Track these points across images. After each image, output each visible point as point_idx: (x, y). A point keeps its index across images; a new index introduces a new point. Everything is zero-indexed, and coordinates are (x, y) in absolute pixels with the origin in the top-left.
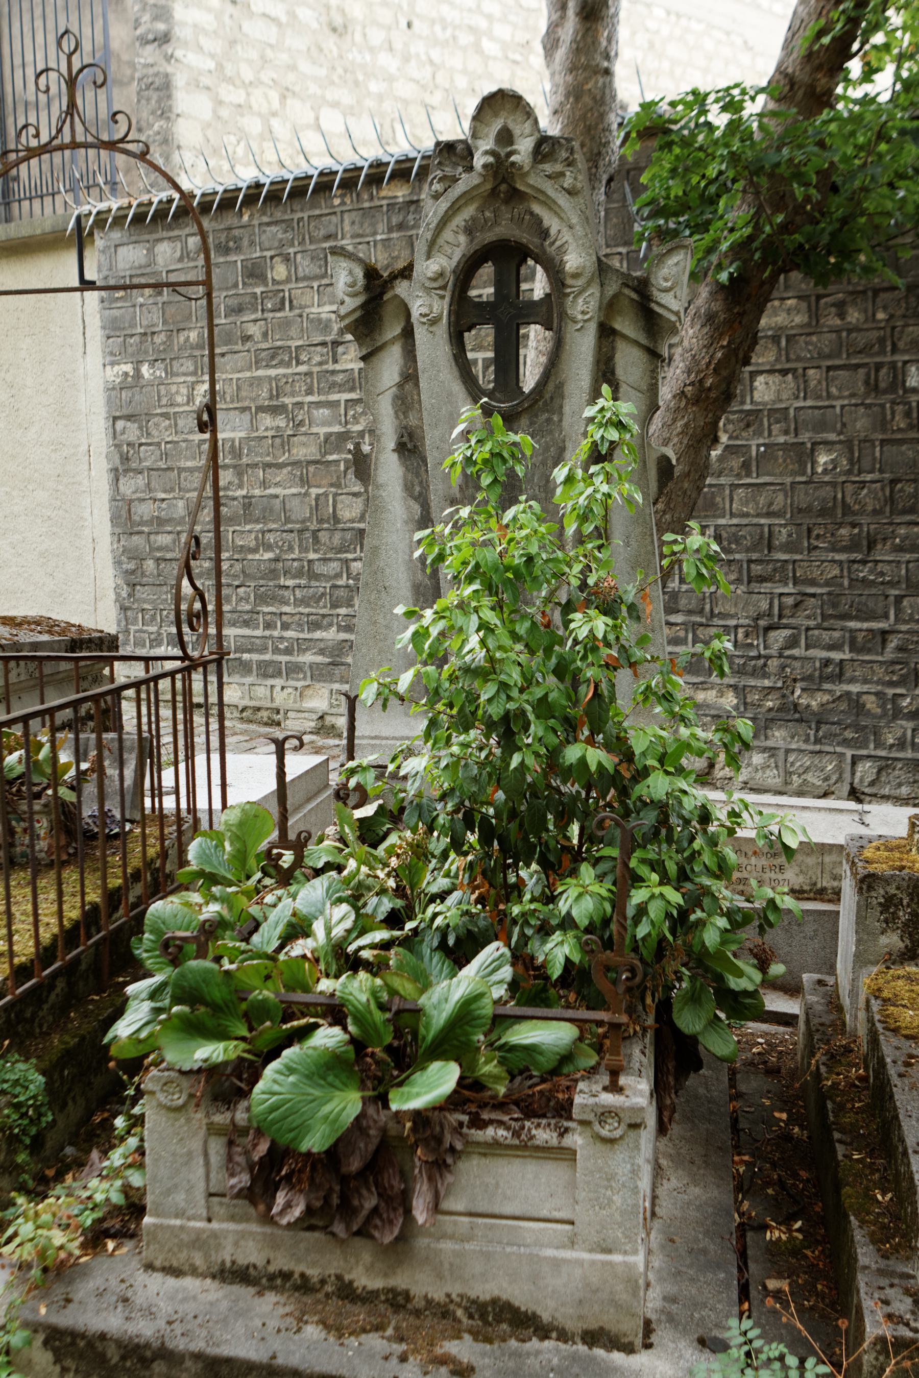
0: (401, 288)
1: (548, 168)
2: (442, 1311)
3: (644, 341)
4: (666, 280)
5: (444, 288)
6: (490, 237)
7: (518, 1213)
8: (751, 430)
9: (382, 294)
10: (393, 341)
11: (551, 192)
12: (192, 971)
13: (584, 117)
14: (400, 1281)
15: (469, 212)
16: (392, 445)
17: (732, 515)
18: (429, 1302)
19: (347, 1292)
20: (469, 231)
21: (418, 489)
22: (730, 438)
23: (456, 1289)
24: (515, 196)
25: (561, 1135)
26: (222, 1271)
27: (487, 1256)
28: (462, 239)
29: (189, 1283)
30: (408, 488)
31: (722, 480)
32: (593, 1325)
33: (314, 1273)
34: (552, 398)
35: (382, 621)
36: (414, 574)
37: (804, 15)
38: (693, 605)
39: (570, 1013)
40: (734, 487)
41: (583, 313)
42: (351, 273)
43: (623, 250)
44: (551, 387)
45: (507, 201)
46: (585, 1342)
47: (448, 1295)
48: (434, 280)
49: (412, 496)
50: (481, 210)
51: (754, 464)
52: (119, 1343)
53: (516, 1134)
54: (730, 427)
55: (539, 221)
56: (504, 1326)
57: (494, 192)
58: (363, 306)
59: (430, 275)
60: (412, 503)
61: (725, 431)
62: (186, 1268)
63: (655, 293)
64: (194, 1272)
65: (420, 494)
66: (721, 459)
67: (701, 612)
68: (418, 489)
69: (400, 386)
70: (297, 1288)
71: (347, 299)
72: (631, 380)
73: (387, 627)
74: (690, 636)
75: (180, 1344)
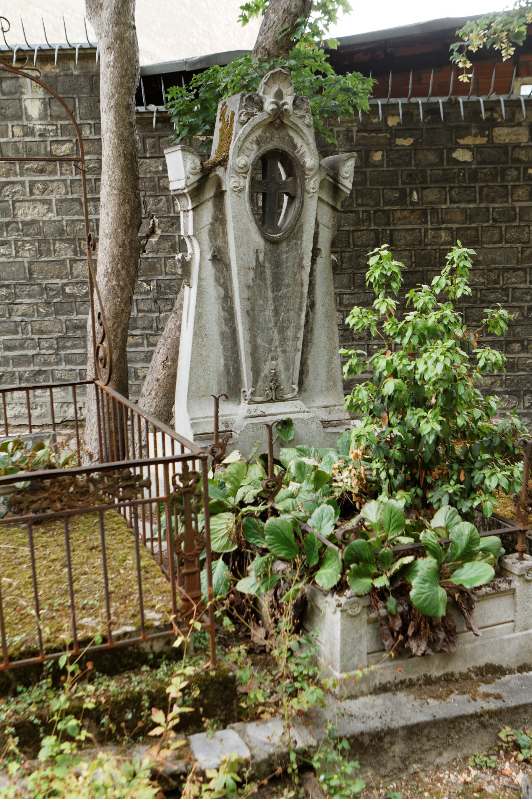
0: (220, 171)
1: (299, 113)
2: (465, 677)
3: (331, 203)
4: (347, 173)
5: (246, 173)
6: (270, 146)
7: (494, 623)
8: (174, 227)
9: (209, 174)
10: (208, 200)
11: (300, 126)
12: (356, 546)
13: (126, 53)
14: (450, 669)
15: (258, 133)
16: (209, 257)
17: (166, 274)
18: (461, 674)
19: (428, 681)
20: (259, 142)
21: (222, 280)
22: (162, 231)
23: (471, 665)
24: (282, 126)
25: (510, 584)
26: (375, 690)
27: (484, 646)
28: (255, 147)
29: (362, 700)
30: (217, 280)
31: (160, 255)
32: (521, 663)
33: (414, 677)
35: (204, 353)
36: (221, 327)
37: (275, 19)
38: (146, 324)
39: (493, 532)
40: (166, 258)
41: (313, 189)
42: (193, 162)
43: (92, 122)
44: (297, 227)
45: (277, 129)
46: (519, 671)
47: (469, 669)
48: (241, 168)
50: (264, 132)
51: (177, 246)
52: (369, 734)
53: (493, 588)
54: (162, 226)
55: (292, 139)
56: (489, 675)
57: (271, 124)
58: (199, 181)
59: (240, 165)
61: (159, 228)
62: (359, 693)
63: (341, 179)
64: (363, 694)
65: (224, 283)
66: (158, 243)
67: (151, 328)
68: (222, 280)
69: (212, 224)
70: (408, 687)
71: (191, 176)
73: (207, 356)
74: (145, 342)
75: (395, 725)
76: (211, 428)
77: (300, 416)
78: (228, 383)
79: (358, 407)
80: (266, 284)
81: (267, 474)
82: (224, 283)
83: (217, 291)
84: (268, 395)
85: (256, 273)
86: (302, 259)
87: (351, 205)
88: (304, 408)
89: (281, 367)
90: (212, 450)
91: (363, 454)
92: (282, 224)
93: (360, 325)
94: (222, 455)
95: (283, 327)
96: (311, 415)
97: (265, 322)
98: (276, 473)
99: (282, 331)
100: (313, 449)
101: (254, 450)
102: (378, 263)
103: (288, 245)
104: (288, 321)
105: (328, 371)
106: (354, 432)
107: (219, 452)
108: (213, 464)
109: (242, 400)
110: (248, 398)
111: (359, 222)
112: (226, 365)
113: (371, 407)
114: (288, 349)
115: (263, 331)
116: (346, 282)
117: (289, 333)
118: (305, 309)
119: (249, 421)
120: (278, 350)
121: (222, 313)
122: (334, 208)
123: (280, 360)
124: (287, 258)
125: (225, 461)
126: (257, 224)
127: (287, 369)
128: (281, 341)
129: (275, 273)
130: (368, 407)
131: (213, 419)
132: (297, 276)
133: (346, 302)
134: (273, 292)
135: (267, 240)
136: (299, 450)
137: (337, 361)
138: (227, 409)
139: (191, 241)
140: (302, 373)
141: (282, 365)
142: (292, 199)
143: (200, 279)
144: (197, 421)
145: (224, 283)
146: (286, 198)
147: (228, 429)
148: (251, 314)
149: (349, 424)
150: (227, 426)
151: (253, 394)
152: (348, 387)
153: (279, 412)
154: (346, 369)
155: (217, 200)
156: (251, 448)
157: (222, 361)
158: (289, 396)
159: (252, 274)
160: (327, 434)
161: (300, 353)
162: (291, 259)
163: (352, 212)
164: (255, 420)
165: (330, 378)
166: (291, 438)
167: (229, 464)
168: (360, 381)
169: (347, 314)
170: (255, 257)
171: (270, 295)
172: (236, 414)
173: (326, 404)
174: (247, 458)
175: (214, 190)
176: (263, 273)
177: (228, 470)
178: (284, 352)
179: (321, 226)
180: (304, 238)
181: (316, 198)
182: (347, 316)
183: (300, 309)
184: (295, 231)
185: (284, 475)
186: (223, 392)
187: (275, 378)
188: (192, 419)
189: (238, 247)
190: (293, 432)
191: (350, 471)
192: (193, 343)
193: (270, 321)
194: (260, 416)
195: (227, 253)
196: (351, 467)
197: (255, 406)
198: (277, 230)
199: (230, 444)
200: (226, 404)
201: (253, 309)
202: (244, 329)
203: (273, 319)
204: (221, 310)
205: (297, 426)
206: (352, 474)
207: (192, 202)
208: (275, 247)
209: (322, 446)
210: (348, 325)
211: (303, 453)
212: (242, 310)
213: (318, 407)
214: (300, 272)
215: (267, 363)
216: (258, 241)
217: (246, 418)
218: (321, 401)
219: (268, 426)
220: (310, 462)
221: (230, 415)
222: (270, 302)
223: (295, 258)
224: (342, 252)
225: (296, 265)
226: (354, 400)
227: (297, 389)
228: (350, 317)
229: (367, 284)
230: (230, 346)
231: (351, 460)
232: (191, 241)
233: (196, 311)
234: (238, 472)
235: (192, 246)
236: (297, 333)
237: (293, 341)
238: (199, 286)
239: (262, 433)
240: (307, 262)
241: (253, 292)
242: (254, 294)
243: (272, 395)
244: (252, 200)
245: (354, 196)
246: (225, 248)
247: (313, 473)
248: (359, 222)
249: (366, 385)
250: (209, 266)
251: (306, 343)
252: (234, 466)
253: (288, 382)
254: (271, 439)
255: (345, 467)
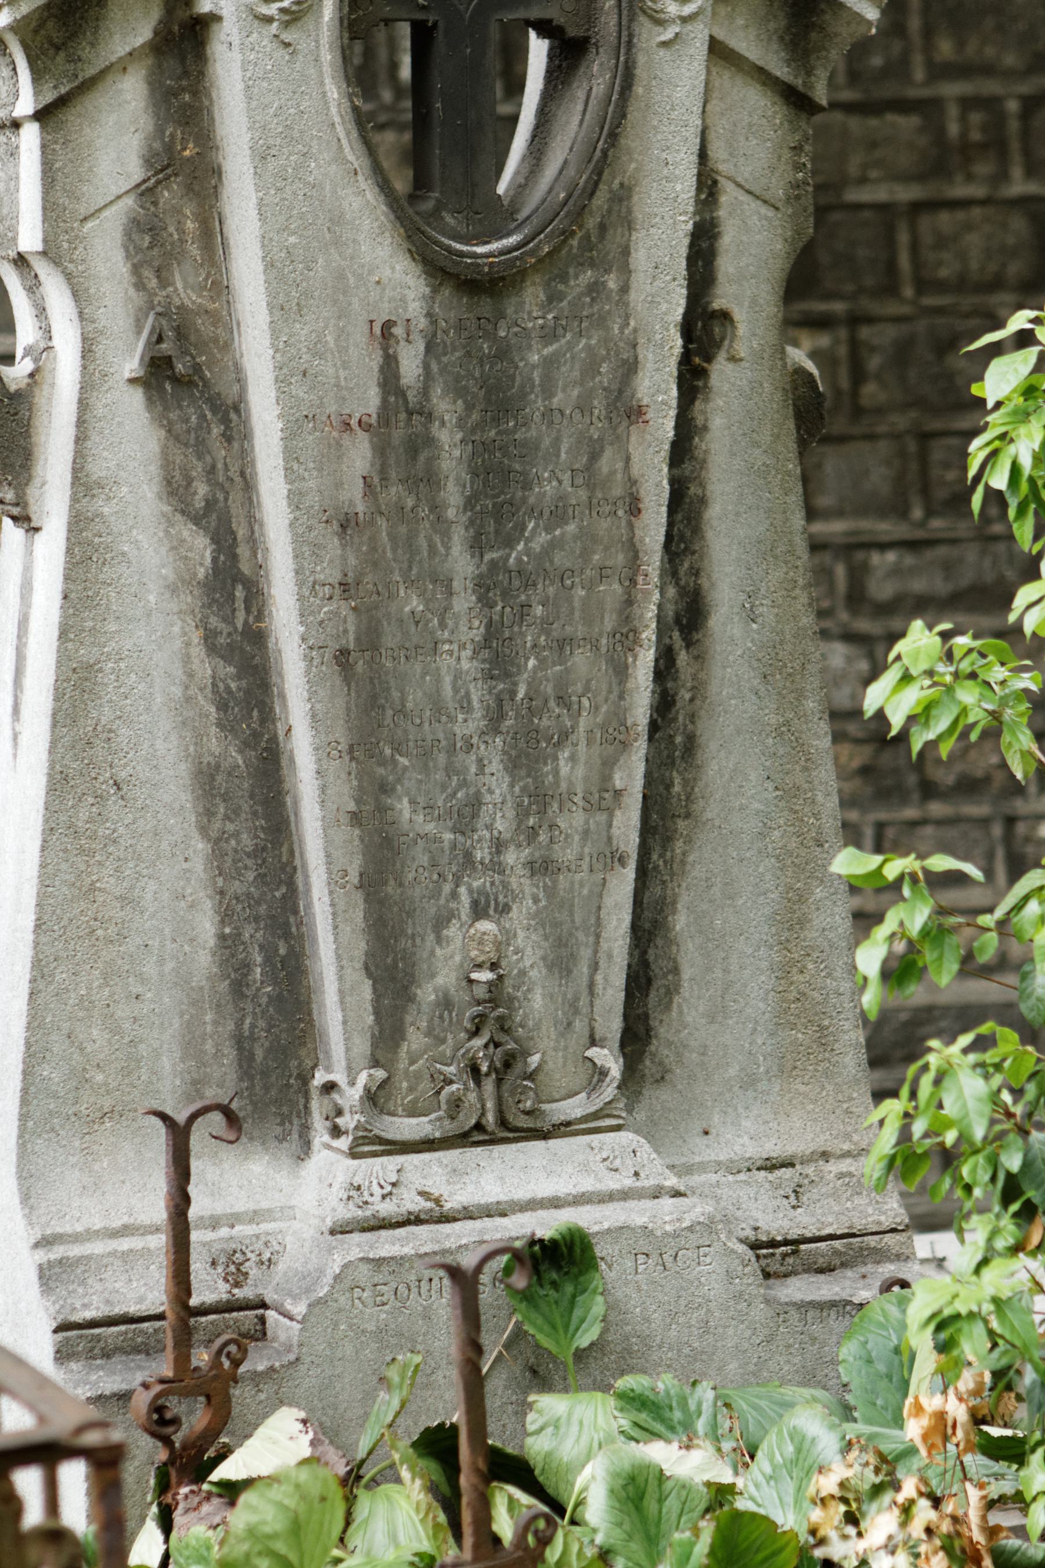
3: (781, 70)
10: (121, 66)
16: (132, 365)
21: (202, 489)
30: (175, 489)
34: (603, 228)
35: (108, 883)
36: (199, 738)
44: (600, 200)
49: (185, 511)
60: (187, 531)
65: (210, 504)
68: (202, 489)
69: (146, 192)
72: (745, 172)
73: (124, 900)
76: (147, 1291)
77: (636, 1214)
78: (242, 1043)
79: (948, 1158)
80: (436, 508)
81: (458, 1536)
82: (212, 500)
83: (177, 546)
84: (456, 1104)
85: (381, 450)
86: (630, 368)
87: (898, 69)
88: (657, 1172)
89: (528, 953)
90: (158, 1409)
91: (978, 1419)
92: (521, 188)
93: (941, 724)
94: (211, 1433)
95: (533, 735)
96: (696, 1210)
97: (439, 709)
98: (504, 1526)
99: (528, 756)
100: (705, 1394)
101: (388, 1403)
102: (1029, 391)
103: (553, 298)
104: (562, 700)
105: (785, 971)
106: (925, 1300)
107: (194, 1418)
108: (164, 1486)
109: (320, 1136)
110: (347, 1121)
111: (941, 160)
112: (228, 944)
113: (1013, 1162)
114: (566, 854)
115: (425, 754)
116: (879, 478)
117: (571, 768)
118: (649, 634)
119: (357, 1245)
120: (511, 857)
121: (204, 668)
122: (797, 100)
123: (519, 915)
124: (550, 363)
125: (227, 1471)
126: (384, 186)
127: (560, 963)
128: (522, 814)
129: (486, 447)
130: (994, 1163)
131: (160, 1242)
132: (609, 461)
133: (881, 589)
134: (477, 546)
135: (441, 271)
136: (632, 1401)
137: (833, 916)
138: (233, 1183)
139: (33, 285)
140: (641, 981)
141: (534, 940)
142: (569, 53)
143: (82, 483)
144: (75, 1251)
145: (212, 500)
146: (538, 51)
147: (245, 1293)
148: (358, 664)
149: (904, 1257)
150: (237, 1277)
151: (375, 1099)
152: (894, 1049)
153: (522, 1194)
154: (870, 958)
155: (171, 63)
156: (369, 1397)
157: (206, 926)
158: (574, 1108)
159: (359, 456)
160: (782, 1310)
161: (630, 873)
162: (568, 372)
163: (902, 106)
164: (389, 1245)
165: (800, 1010)
166: (584, 1340)
167: (248, 1483)
168: (961, 1018)
169: (874, 652)
170: (376, 361)
171: (462, 564)
172: (287, 1212)
173: (772, 1148)
174: (344, 1449)
175: (156, 14)
176: (420, 445)
177: (240, 1518)
178: (542, 867)
179: (729, 195)
180: (640, 258)
181: (699, 48)
182: (873, 676)
183: (626, 637)
184: (589, 222)
185: (544, 1541)
186: (213, 1094)
187: (493, 1012)
188: (44, 1242)
189: (284, 310)
190: (598, 1307)
191: (907, 1510)
192: (49, 831)
193: (466, 707)
194: (414, 1220)
195: (227, 346)
196: (909, 1488)
197: (387, 1166)
198: (495, 218)
199: (256, 1378)
200: (228, 1155)
201: (370, 639)
202: (323, 750)
203: (477, 693)
204: (198, 651)
205: (617, 1272)
206: (917, 1529)
207: (38, 76)
208: (486, 306)
209: (755, 1376)
210: (880, 715)
211: (652, 1415)
212: (312, 649)
213: (732, 1168)
214: (621, 442)
215: (452, 931)
216: (392, 278)
217: (340, 1230)
218: (745, 1136)
219: (455, 1273)
220: (688, 1464)
221: (255, 1216)
222: (464, 602)
223: (591, 368)
224: (855, 320)
225: (599, 405)
226: (918, 1128)
227: (615, 1068)
228: (890, 678)
229: (977, 501)
230: (247, 841)
231: (911, 1451)
232: (33, 285)
233: (63, 658)
234: (296, 1528)
235: (41, 312)
236: (608, 765)
237: (590, 807)
238: (79, 524)
239: (427, 1315)
240: (657, 385)
241: (371, 550)
242: (373, 561)
243: (482, 1102)
244: (362, 73)
245: (915, 24)
246: (215, 318)
247: (708, 1529)
248: (941, 160)
249: (981, 1044)
250: (129, 412)
251: (663, 819)
252: (276, 1493)
253: (569, 1037)
254: (474, 1348)
255: (877, 1490)
